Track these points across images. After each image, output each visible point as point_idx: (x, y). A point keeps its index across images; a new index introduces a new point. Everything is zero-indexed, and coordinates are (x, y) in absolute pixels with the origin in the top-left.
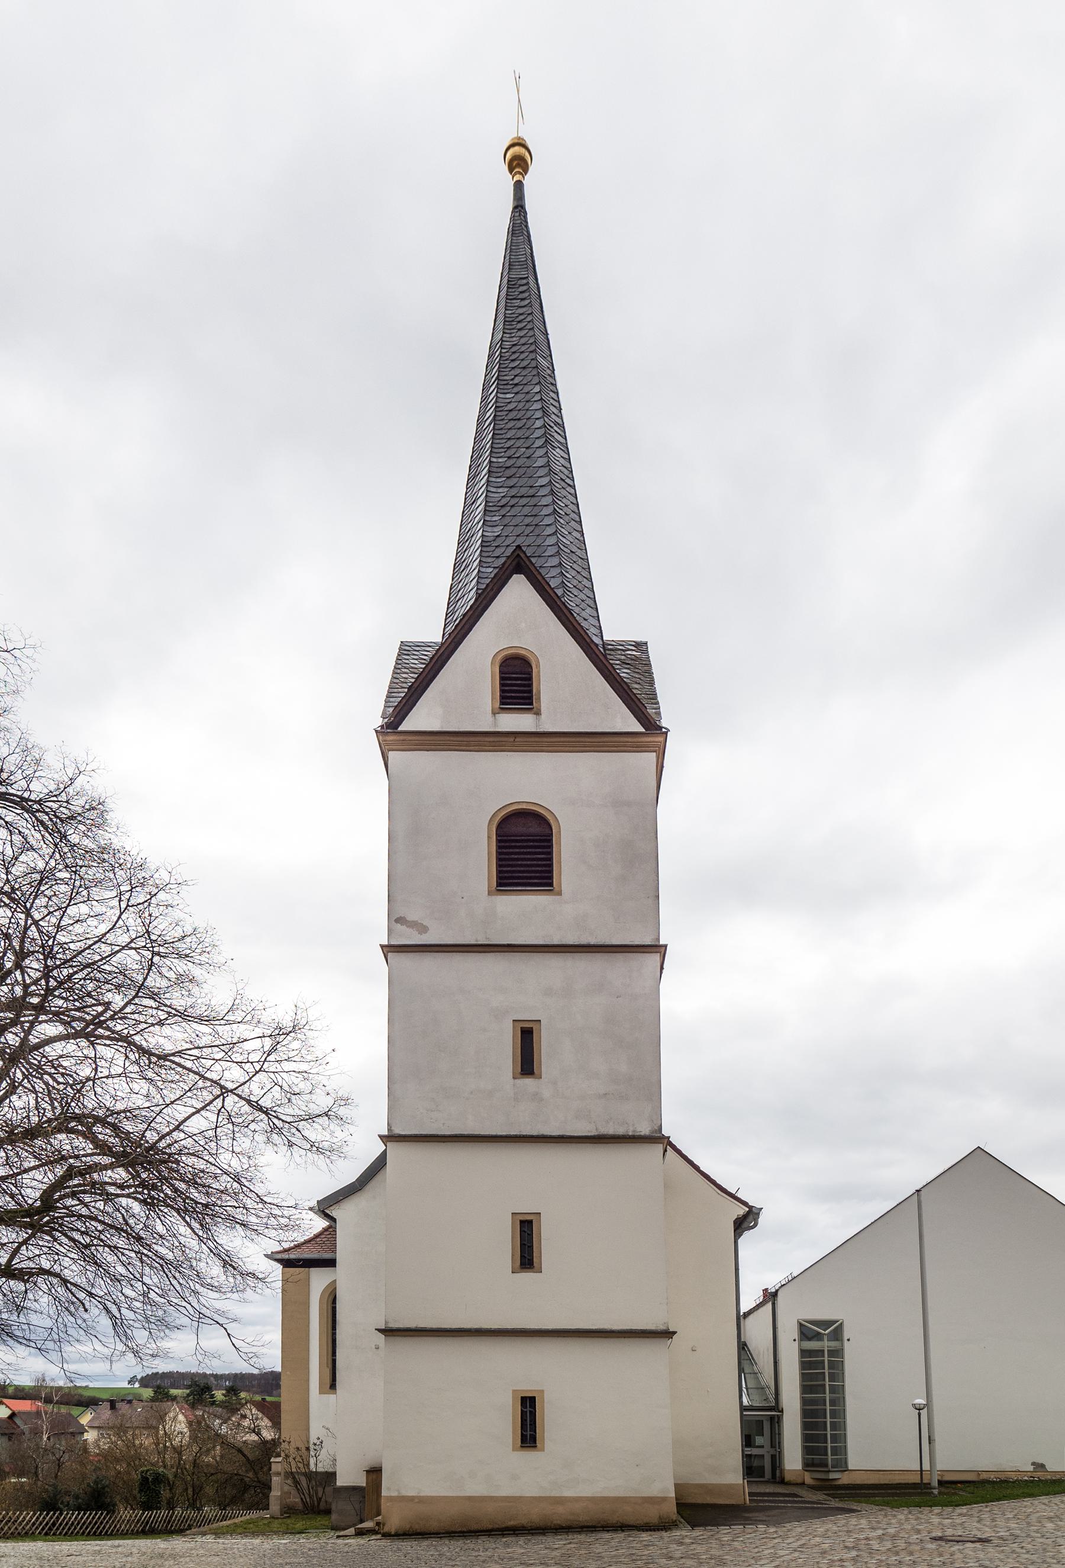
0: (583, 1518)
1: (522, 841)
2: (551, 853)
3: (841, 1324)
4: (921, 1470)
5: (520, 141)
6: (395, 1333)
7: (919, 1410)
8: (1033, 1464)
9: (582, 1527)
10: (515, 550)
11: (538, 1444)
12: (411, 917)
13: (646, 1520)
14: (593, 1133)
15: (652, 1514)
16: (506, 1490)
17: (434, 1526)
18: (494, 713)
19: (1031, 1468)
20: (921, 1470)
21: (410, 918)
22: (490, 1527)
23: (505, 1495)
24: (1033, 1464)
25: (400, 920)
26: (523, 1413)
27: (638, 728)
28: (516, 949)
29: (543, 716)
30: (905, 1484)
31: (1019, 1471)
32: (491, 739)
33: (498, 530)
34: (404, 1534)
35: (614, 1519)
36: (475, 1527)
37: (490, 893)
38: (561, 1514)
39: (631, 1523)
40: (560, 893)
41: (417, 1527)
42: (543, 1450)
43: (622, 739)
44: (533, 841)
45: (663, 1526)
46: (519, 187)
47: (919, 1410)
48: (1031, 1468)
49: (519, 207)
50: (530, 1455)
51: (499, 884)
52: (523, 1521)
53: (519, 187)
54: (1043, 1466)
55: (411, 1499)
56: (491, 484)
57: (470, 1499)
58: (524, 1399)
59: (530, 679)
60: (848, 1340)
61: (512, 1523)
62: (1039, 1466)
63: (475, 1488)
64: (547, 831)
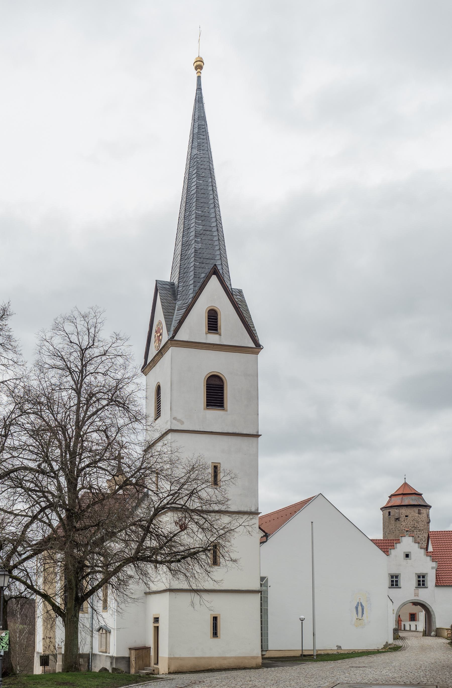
0: (233, 665)
1: (213, 387)
2: (223, 393)
3: (267, 578)
4: (302, 650)
5: (202, 60)
6: (173, 591)
7: (302, 621)
8: (337, 646)
9: (232, 669)
10: (214, 266)
11: (218, 635)
12: (178, 418)
13: (252, 666)
14: (236, 510)
15: (253, 663)
16: (208, 654)
17: (185, 669)
18: (206, 334)
19: (336, 648)
20: (302, 650)
21: (178, 418)
22: (203, 669)
23: (207, 656)
24: (337, 646)
25: (175, 418)
26: (213, 623)
27: (254, 346)
28: (213, 433)
29: (222, 336)
30: (293, 656)
31: (332, 650)
32: (206, 345)
33: (200, 245)
34: (176, 673)
35: (242, 665)
36: (198, 669)
37: (204, 409)
38: (225, 664)
39: (248, 667)
40: (227, 411)
41: (180, 670)
42: (220, 638)
43: (246, 349)
44: (217, 387)
45: (257, 667)
46: (199, 78)
47: (302, 621)
48: (336, 648)
49: (199, 88)
50: (215, 639)
51: (207, 405)
52: (213, 666)
53: (199, 78)
54: (340, 647)
55: (177, 658)
56: (197, 223)
57: (196, 658)
58: (214, 617)
59: (217, 319)
60: (270, 586)
61: (210, 668)
62: (339, 647)
63: (198, 654)
64: (222, 384)
